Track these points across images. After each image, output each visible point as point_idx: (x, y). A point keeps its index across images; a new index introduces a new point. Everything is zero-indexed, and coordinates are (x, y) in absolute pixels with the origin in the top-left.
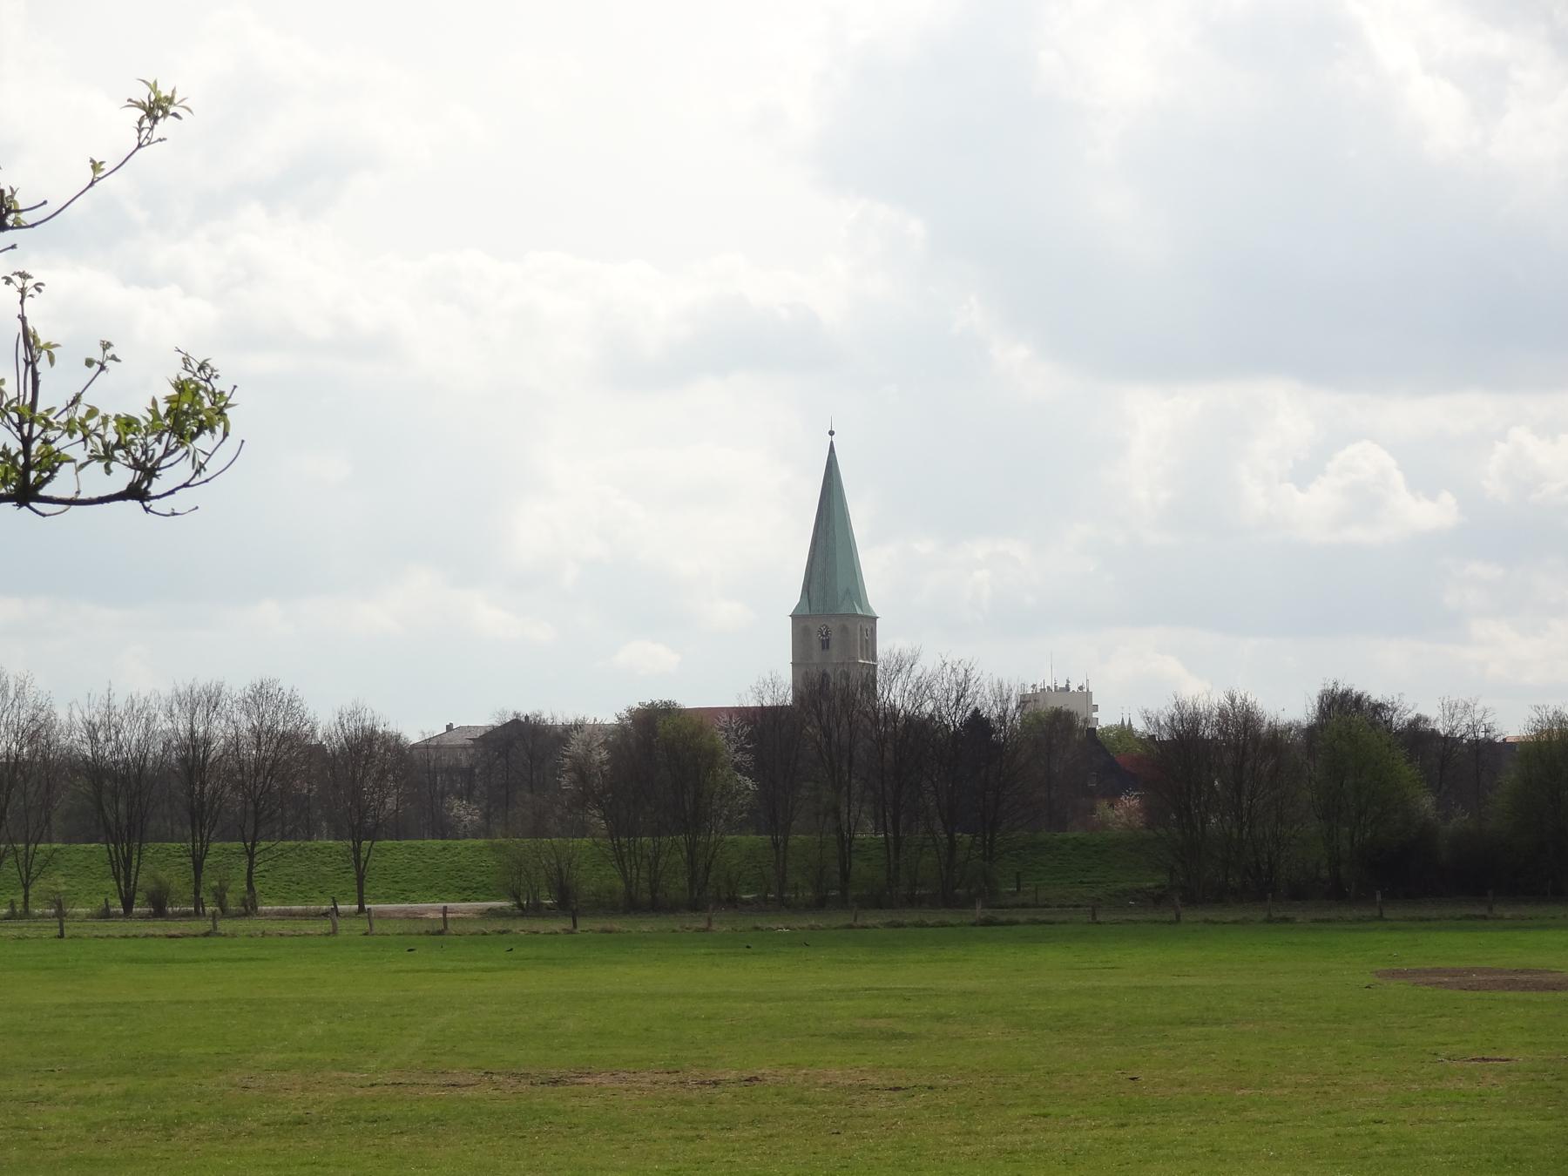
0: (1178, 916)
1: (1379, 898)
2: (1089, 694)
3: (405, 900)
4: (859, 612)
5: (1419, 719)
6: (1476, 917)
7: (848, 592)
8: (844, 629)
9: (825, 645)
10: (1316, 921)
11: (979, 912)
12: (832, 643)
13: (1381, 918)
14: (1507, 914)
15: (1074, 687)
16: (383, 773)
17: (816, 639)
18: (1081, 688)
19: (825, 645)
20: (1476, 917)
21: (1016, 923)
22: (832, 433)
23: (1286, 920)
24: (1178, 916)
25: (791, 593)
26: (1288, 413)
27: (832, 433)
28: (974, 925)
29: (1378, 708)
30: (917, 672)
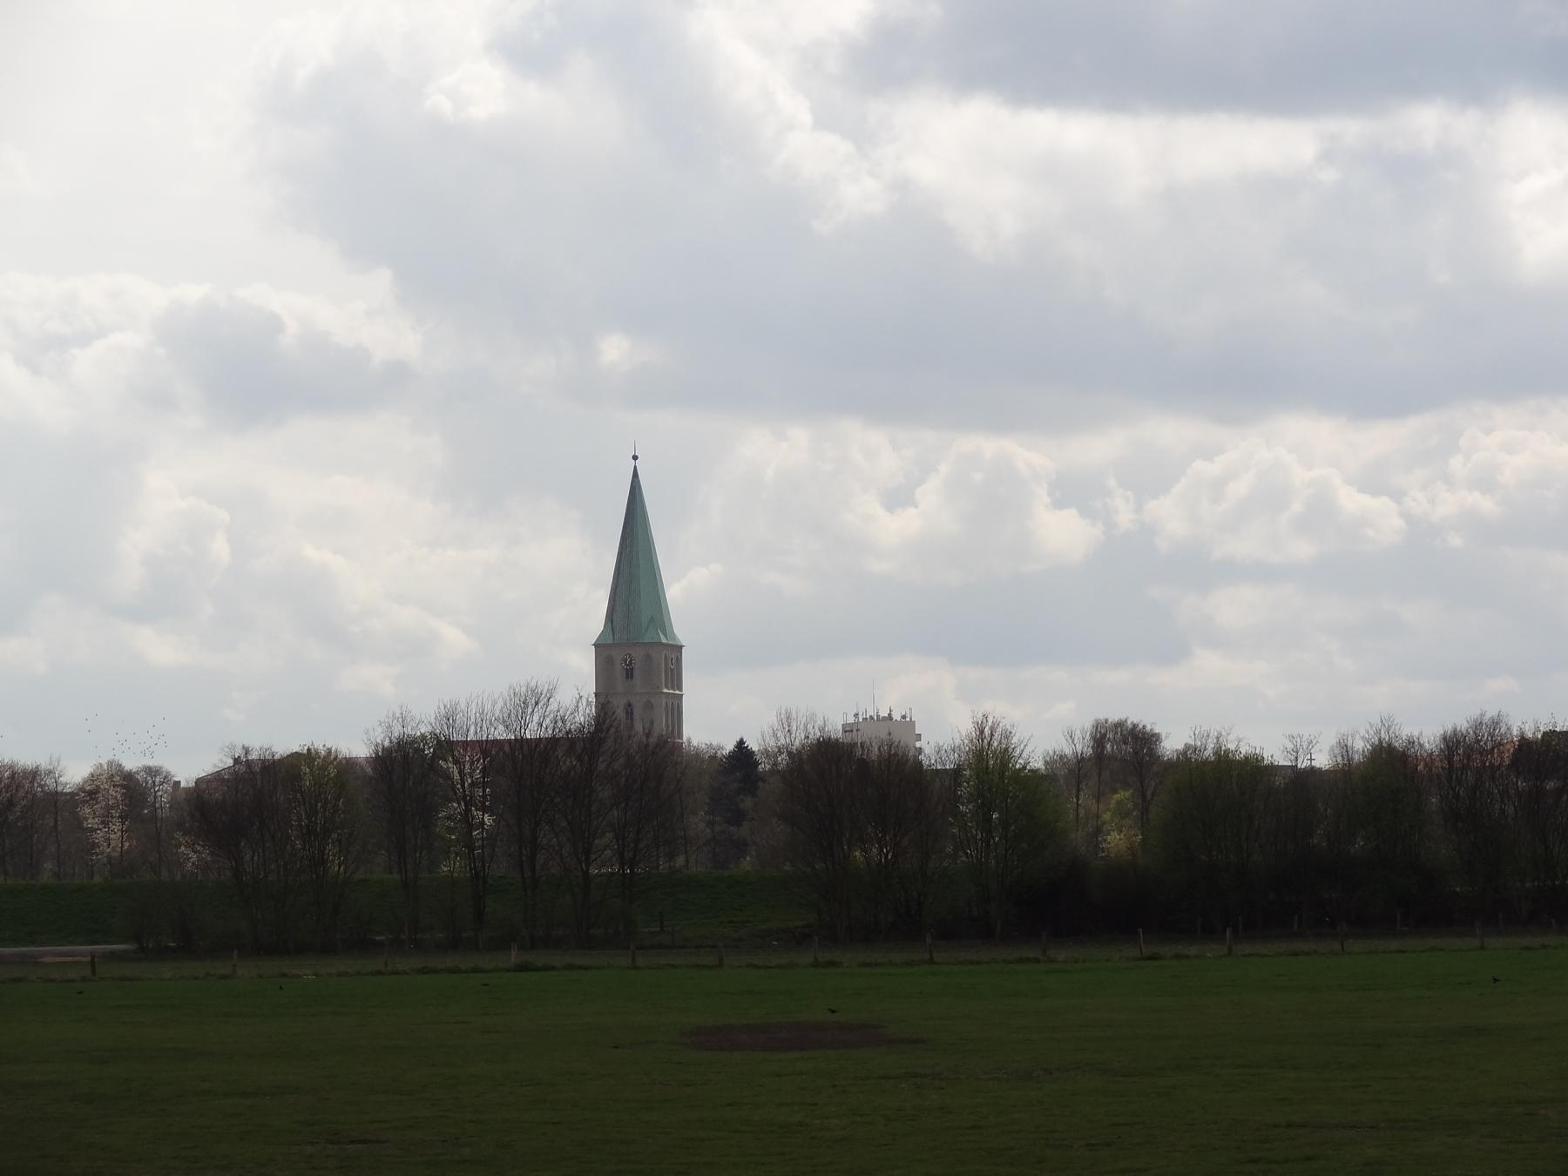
0: (1230, 951)
1: (929, 940)
2: (912, 723)
3: (33, 943)
4: (664, 641)
5: (1097, 726)
6: (1028, 960)
7: (652, 620)
8: (648, 657)
9: (629, 674)
10: (865, 965)
11: (514, 957)
12: (636, 673)
13: (931, 961)
14: (1193, 950)
15: (897, 716)
16: (108, 808)
17: (619, 669)
18: (856, 715)
19: (629, 674)
20: (1028, 960)
21: (553, 968)
22: (635, 458)
23: (832, 964)
24: (1230, 951)
25: (596, 622)
26: (876, 450)
27: (635, 458)
28: (508, 970)
29: (1135, 726)
30: (553, 706)
